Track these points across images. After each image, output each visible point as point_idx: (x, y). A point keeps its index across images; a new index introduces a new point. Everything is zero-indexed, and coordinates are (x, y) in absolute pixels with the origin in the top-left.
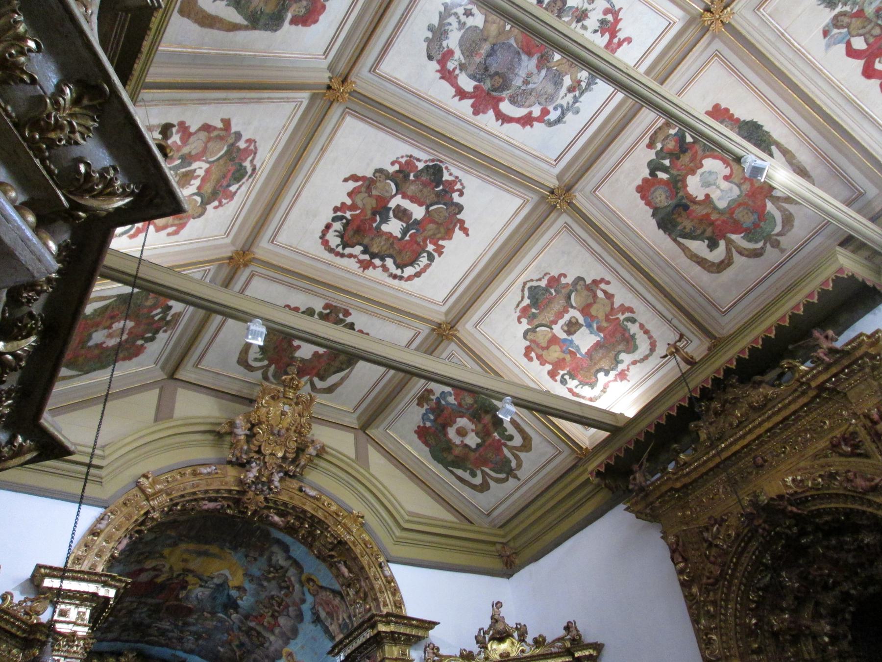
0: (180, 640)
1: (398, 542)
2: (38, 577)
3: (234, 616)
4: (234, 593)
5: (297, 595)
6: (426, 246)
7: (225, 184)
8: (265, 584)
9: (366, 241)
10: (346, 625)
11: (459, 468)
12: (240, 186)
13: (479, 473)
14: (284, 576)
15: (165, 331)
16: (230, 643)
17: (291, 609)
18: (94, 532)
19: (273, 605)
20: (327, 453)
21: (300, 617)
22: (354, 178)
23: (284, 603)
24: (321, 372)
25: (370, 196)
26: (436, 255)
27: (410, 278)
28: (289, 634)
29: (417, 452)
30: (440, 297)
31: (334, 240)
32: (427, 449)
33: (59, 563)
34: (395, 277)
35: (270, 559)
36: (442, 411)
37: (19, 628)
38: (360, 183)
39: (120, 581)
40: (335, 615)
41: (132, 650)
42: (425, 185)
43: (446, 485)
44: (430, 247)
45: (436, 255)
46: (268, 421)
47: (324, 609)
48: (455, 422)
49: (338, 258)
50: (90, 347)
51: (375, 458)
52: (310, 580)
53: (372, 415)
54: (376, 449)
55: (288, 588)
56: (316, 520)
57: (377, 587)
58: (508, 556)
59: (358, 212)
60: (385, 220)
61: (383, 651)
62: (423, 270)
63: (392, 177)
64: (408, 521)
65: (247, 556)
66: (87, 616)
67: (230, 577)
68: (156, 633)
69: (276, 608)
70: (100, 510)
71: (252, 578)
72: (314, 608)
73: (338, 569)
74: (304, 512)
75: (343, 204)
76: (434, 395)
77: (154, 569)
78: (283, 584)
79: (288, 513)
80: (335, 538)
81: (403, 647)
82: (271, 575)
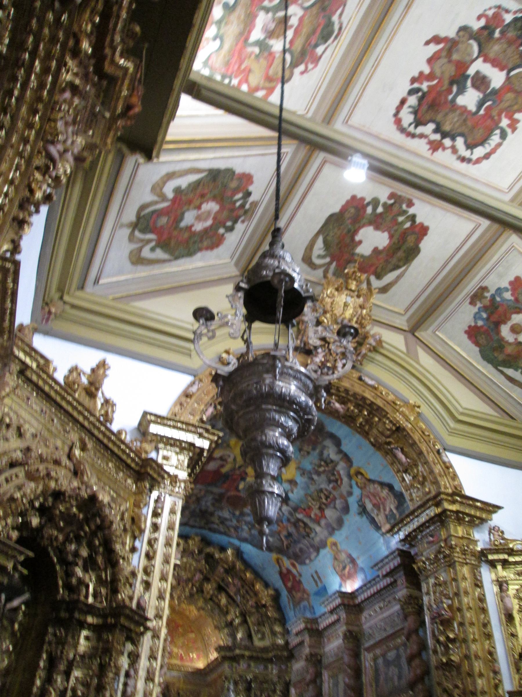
0: (236, 528)
1: (452, 433)
2: (144, 423)
6: (500, 120)
7: (313, 42)
8: (315, 477)
9: (439, 118)
10: (393, 515)
11: (510, 367)
12: (326, 49)
14: (334, 469)
15: (243, 222)
16: (279, 533)
17: (338, 502)
18: (187, 395)
19: (321, 498)
20: (382, 347)
21: (346, 509)
22: (436, 40)
23: (331, 496)
24: (379, 270)
25: (450, 61)
26: (509, 131)
27: (478, 161)
28: (335, 526)
29: (468, 353)
30: (505, 184)
31: (407, 118)
32: (477, 349)
33: (163, 412)
34: (463, 159)
35: (321, 454)
36: (497, 308)
37: (133, 460)
38: (441, 46)
39: (214, 434)
40: (381, 507)
41: (197, 535)
42: (510, 43)
43: (494, 387)
44: (505, 122)
45: (509, 131)
46: (332, 311)
47: (371, 501)
48: (510, 319)
49: (409, 139)
50: (181, 229)
51: (425, 359)
52: (358, 473)
53: (423, 316)
54: (424, 350)
55: (336, 481)
56: (375, 407)
57: (436, 471)
59: (435, 82)
60: (461, 90)
61: (448, 530)
62: (493, 151)
63: (476, 36)
64: (462, 414)
66: (186, 464)
68: (217, 521)
69: (324, 501)
70: (189, 379)
71: (303, 472)
73: (395, 456)
74: (364, 399)
75: (421, 73)
76: (488, 291)
77: (221, 458)
78: (332, 478)
79: (349, 401)
80: (394, 425)
81: (467, 528)
82: (321, 469)
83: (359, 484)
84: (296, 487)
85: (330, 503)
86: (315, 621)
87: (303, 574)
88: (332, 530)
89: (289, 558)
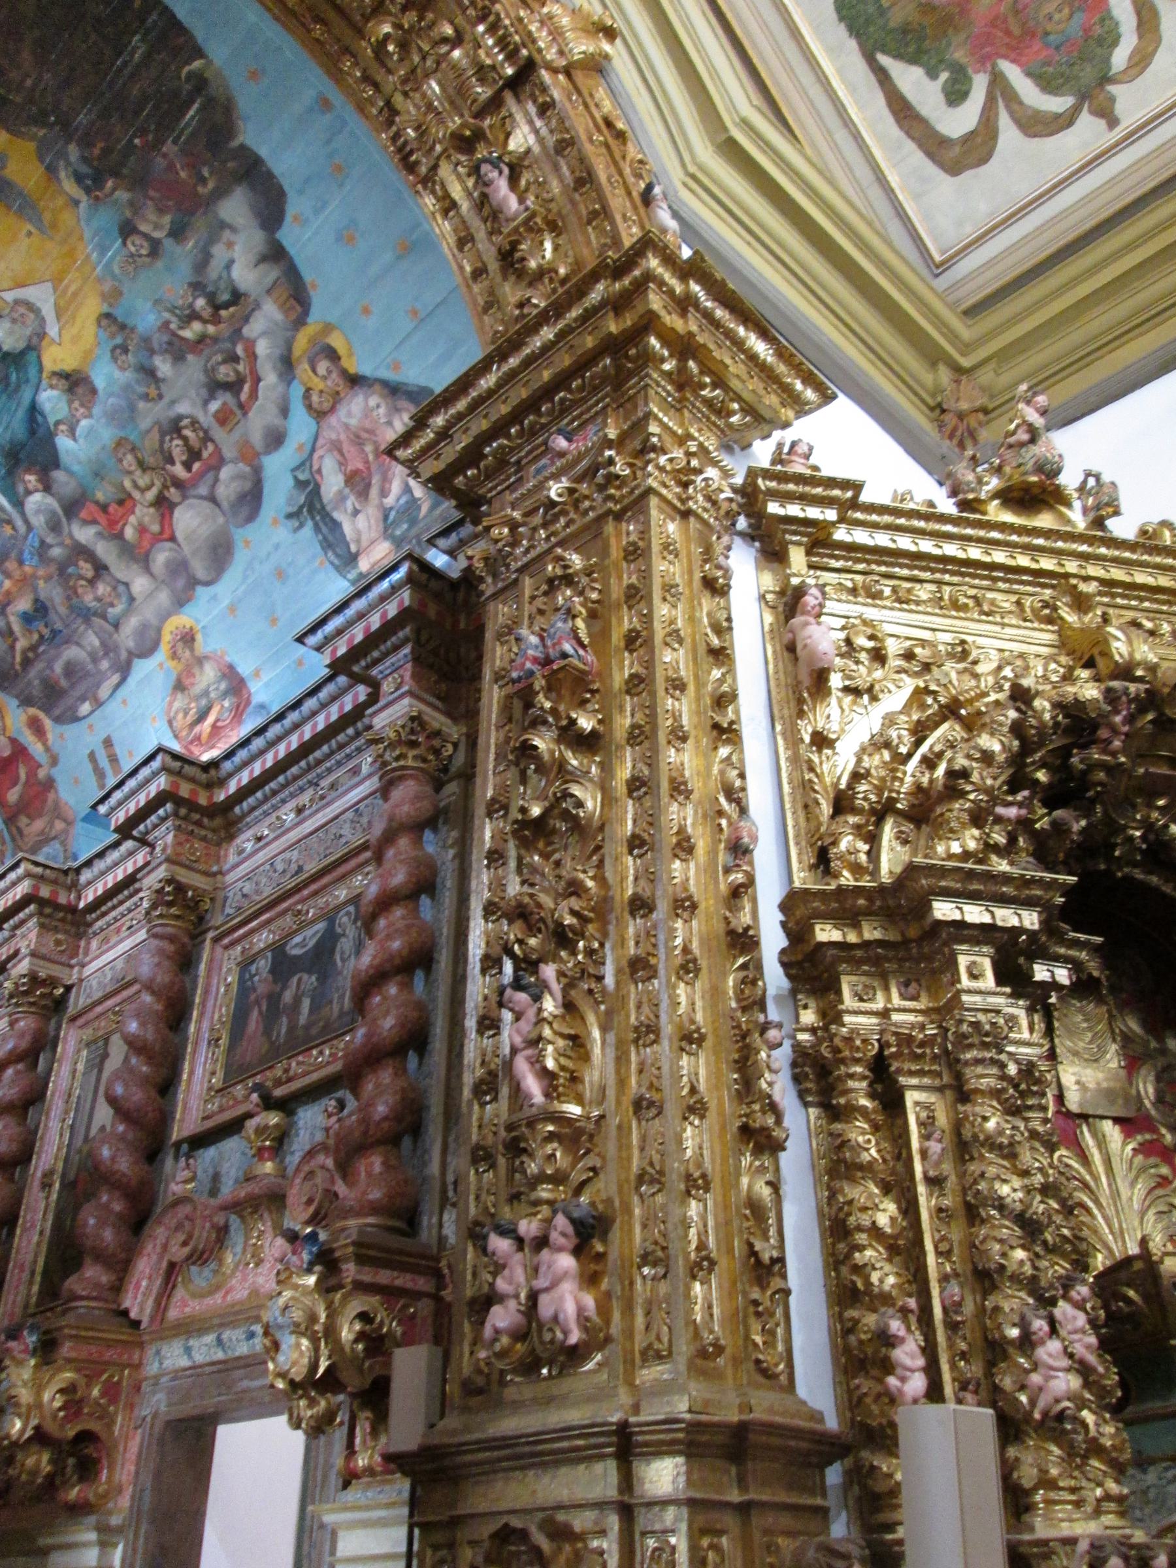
3: (36, 501)
4: (52, 400)
5: (257, 422)
8: (164, 367)
11: (913, 60)
13: (980, 85)
17: (225, 473)
21: (251, 500)
40: (376, 480)
43: (842, 136)
58: (961, 416)
65: (127, 230)
67: (53, 330)
69: (178, 470)
72: (306, 462)
80: (512, 56)
82: (190, 332)
83: (315, 398)
84: (88, 405)
85: (201, 475)
86: (69, 877)
87: (62, 760)
88: (185, 584)
89: (26, 701)
